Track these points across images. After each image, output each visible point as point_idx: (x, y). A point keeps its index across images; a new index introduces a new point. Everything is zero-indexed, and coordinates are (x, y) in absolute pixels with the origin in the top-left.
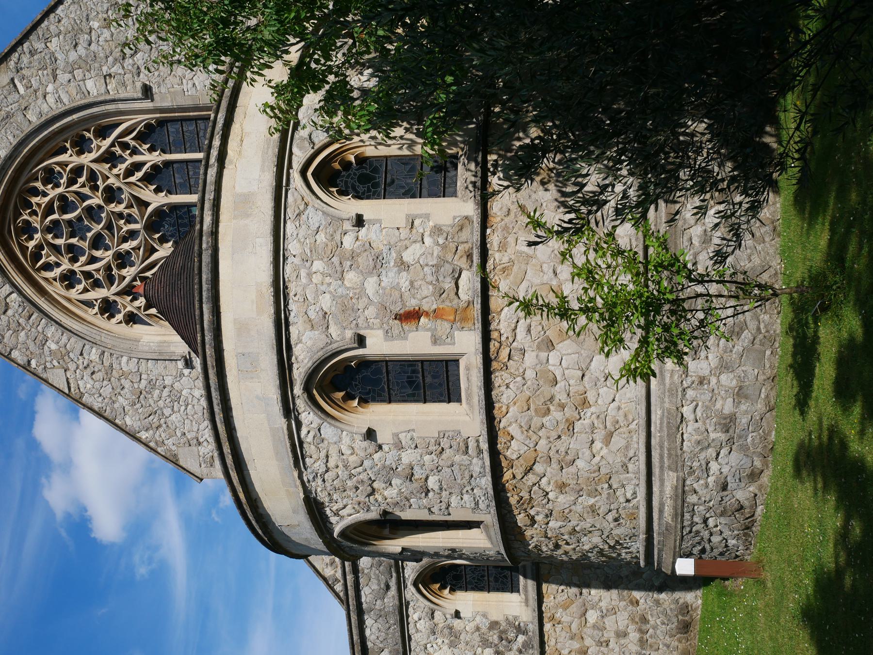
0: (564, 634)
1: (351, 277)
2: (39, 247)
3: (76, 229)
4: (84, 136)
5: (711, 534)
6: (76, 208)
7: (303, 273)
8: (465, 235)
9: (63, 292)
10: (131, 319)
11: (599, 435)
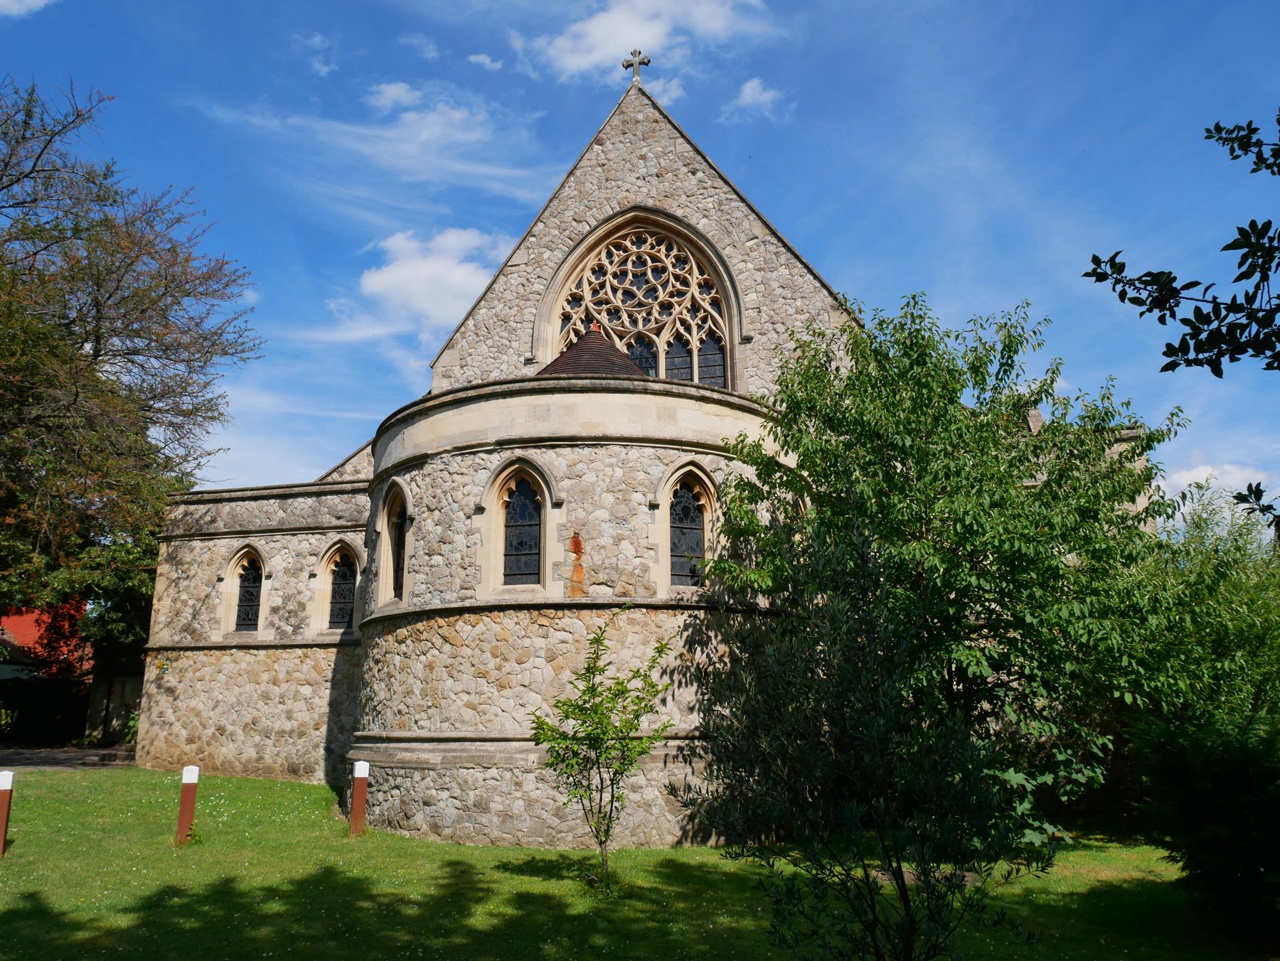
0: (292, 665)
1: (609, 499)
2: (626, 250)
3: (639, 278)
4: (712, 288)
5: (384, 792)
6: (656, 280)
7: (613, 460)
8: (641, 591)
9: (589, 266)
10: (566, 318)
11: (474, 699)
